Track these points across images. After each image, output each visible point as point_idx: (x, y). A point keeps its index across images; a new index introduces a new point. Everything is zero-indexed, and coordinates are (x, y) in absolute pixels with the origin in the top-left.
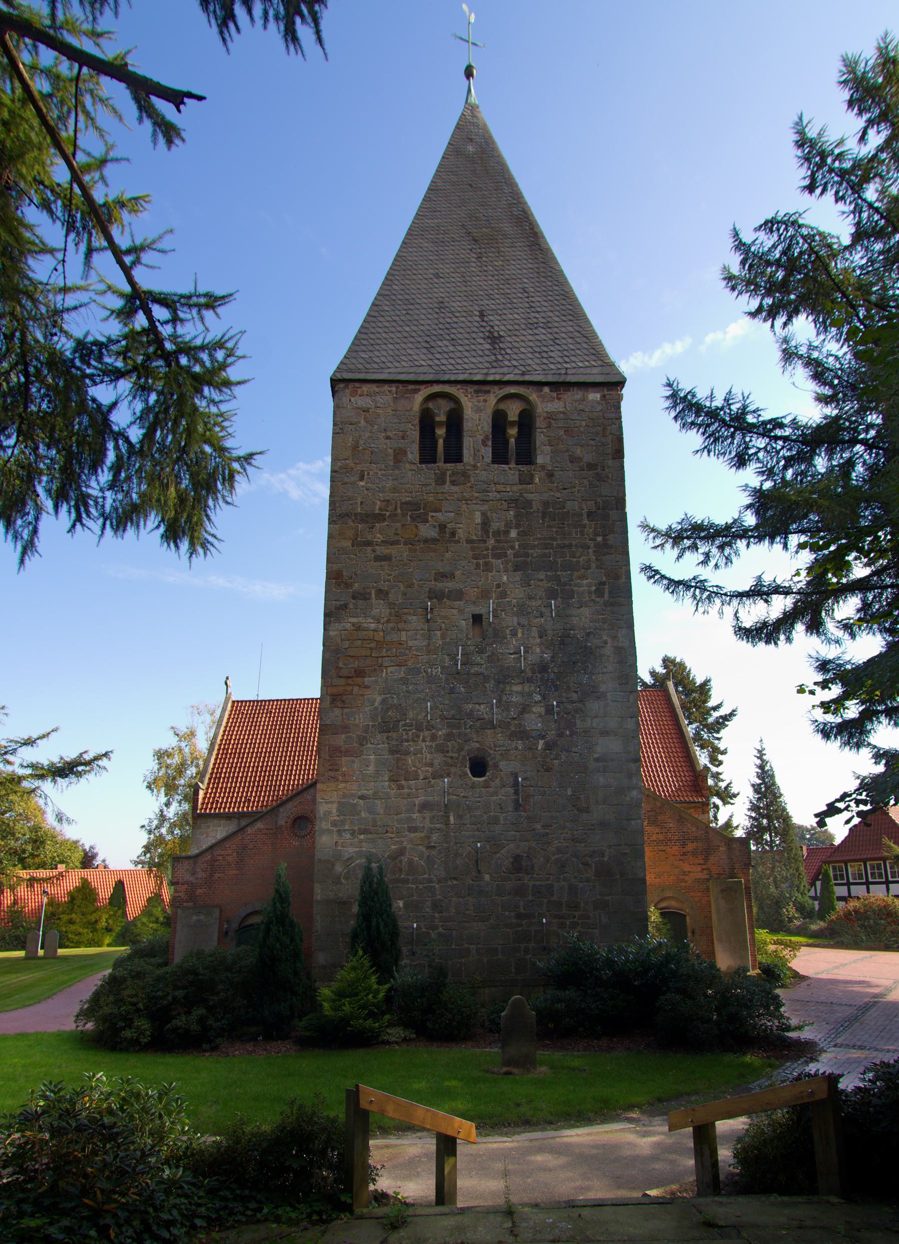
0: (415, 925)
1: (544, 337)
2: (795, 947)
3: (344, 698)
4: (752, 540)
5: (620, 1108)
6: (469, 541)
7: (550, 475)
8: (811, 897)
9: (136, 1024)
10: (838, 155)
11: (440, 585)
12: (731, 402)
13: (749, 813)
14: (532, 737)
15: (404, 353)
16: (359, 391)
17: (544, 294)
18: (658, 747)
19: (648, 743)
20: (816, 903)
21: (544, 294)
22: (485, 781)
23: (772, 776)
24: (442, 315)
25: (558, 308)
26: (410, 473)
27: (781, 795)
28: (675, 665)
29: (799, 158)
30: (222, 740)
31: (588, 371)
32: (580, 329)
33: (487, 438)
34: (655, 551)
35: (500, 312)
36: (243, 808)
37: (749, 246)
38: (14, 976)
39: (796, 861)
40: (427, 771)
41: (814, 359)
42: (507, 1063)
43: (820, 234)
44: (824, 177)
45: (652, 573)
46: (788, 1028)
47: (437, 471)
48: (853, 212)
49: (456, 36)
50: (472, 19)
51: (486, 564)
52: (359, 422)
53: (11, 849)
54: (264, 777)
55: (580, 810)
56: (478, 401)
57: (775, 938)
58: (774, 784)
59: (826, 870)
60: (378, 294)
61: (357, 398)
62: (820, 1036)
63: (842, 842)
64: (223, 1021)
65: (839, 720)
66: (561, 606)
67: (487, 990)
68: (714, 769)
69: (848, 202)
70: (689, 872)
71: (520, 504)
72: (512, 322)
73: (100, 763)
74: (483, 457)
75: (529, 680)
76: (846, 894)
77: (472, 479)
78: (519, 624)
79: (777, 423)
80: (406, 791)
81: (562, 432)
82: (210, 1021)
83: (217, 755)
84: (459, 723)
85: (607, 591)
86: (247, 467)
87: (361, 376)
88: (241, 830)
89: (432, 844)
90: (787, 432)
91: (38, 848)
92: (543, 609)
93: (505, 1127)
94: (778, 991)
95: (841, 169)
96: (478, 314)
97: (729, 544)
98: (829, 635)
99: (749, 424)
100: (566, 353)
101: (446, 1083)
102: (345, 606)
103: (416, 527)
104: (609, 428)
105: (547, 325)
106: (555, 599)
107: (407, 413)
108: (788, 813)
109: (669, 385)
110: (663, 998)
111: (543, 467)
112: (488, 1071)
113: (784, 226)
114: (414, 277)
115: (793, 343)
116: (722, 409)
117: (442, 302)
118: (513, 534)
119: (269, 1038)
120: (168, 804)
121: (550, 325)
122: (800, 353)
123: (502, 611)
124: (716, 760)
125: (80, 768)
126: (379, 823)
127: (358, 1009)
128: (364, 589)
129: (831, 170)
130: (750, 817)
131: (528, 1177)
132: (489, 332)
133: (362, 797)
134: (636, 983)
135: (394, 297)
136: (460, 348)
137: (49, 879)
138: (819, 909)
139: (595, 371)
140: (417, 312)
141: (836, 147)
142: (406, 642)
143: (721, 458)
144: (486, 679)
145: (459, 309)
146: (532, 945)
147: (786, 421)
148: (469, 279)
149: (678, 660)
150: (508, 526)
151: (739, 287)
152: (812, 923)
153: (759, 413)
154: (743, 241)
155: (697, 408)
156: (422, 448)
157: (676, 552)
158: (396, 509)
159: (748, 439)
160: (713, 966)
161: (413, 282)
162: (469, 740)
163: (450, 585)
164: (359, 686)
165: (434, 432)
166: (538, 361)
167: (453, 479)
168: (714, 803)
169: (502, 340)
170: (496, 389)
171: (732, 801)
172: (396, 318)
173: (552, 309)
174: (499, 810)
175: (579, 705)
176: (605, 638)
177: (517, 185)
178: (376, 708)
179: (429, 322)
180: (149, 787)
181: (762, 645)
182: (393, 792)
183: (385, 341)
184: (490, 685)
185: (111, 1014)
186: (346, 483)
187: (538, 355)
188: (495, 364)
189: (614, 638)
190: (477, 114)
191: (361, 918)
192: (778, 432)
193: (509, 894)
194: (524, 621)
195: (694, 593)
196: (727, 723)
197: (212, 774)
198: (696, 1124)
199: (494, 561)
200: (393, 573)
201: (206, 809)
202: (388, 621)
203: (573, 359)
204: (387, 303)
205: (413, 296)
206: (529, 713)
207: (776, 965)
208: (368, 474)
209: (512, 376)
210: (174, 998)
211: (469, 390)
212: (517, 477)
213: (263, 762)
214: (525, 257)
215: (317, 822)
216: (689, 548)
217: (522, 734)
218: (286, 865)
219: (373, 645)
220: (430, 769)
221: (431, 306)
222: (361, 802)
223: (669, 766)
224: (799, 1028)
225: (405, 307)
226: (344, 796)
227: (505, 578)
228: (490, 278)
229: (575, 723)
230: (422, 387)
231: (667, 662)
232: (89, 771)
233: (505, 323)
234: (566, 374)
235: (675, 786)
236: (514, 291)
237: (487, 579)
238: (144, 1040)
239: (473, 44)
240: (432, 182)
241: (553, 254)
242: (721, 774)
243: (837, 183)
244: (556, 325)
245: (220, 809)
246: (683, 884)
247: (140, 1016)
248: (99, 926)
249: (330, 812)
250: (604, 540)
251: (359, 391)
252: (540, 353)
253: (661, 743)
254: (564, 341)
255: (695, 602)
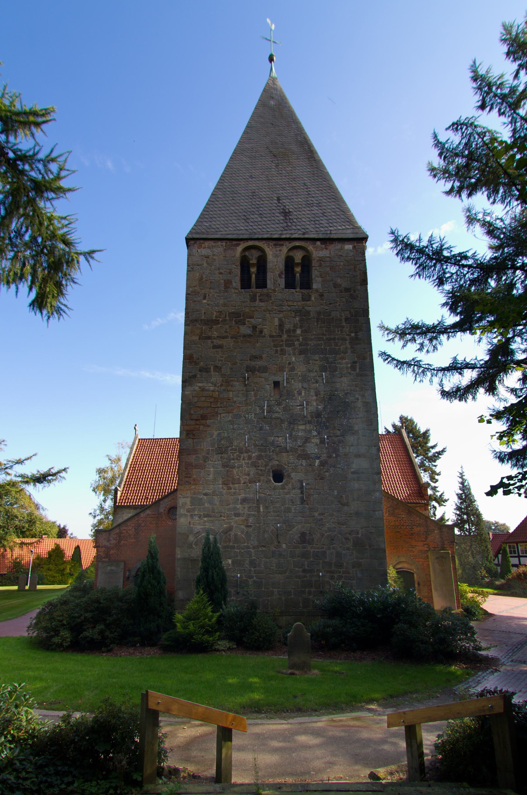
0: (239, 575)
1: (317, 212)
2: (485, 595)
3: (194, 432)
4: (450, 334)
5: (364, 702)
6: (271, 336)
7: (321, 295)
8: (495, 564)
9: (61, 633)
10: (500, 84)
11: (253, 363)
12: (432, 242)
13: (455, 512)
14: (312, 458)
15: (231, 222)
16: (203, 245)
17: (317, 186)
18: (396, 469)
19: (390, 466)
20: (499, 568)
21: (317, 186)
22: (283, 485)
23: (469, 489)
24: (254, 200)
25: (325, 195)
26: (234, 295)
27: (475, 501)
28: (407, 421)
29: (474, 88)
30: (132, 462)
31: (345, 231)
32: (339, 207)
33: (282, 273)
34: (389, 342)
35: (290, 197)
36: (144, 502)
37: (444, 145)
38: (7, 601)
39: (485, 541)
40: (246, 478)
41: (487, 222)
42: (293, 666)
43: (489, 131)
44: (491, 100)
45: (386, 356)
46: (480, 649)
47: (251, 294)
48: (511, 123)
49: (263, 38)
50: (273, 27)
51: (282, 350)
52: (203, 264)
53: (16, 526)
54: (157, 484)
55: (343, 505)
56: (276, 251)
57: (472, 589)
58: (470, 494)
59: (505, 548)
60: (215, 188)
61: (202, 249)
62: (501, 654)
63: (515, 531)
64: (115, 633)
65: (509, 450)
66: (329, 376)
67: (284, 618)
68: (433, 484)
69: (507, 115)
70: (416, 546)
71: (303, 314)
72: (297, 203)
73: (61, 474)
74: (279, 285)
75: (310, 422)
76: (517, 563)
77: (273, 298)
78: (303, 387)
79: (463, 256)
80: (233, 490)
81: (328, 269)
82: (107, 633)
83: (129, 470)
84: (266, 449)
85: (358, 367)
86: (90, 259)
87: (204, 236)
88: (137, 514)
89: (250, 524)
90: (470, 262)
91: (32, 526)
92: (318, 378)
93: (285, 712)
94: (472, 624)
95: (501, 94)
96: (276, 198)
97: (436, 338)
98: (500, 396)
99: (445, 257)
100: (330, 221)
101: (251, 680)
102: (195, 376)
103: (238, 328)
104: (358, 266)
105: (319, 205)
106: (325, 372)
107: (232, 258)
108: (479, 512)
109: (393, 233)
110: (395, 626)
111: (317, 291)
112: (279, 672)
113: (465, 127)
114: (237, 178)
115: (474, 212)
116: (427, 247)
117: (254, 192)
118: (299, 332)
119: (143, 645)
120: (105, 501)
121: (320, 205)
122: (478, 218)
123: (292, 379)
124: (434, 479)
125: (50, 478)
126: (216, 511)
127: (199, 628)
128: (206, 365)
129: (495, 95)
130: (456, 514)
131: (293, 752)
132: (283, 209)
133: (205, 494)
134: (379, 616)
135: (224, 190)
136: (265, 219)
137: (31, 544)
138: (501, 572)
139: (349, 231)
140: (239, 198)
141: (498, 79)
142: (233, 398)
143: (427, 280)
144: (282, 421)
145: (265, 196)
146: (313, 590)
147: (469, 254)
148: (270, 178)
149: (409, 418)
150: (295, 327)
151: (439, 175)
152: (496, 580)
153: (451, 249)
154: (440, 141)
155: (410, 247)
156: (242, 280)
157: (402, 343)
158: (226, 317)
159: (445, 267)
160: (429, 606)
161: (237, 181)
162: (272, 459)
163: (260, 363)
164: (204, 425)
165: (249, 271)
166: (313, 226)
167: (261, 298)
168: (433, 505)
169: (291, 214)
170: (287, 243)
171: (444, 504)
172: (226, 202)
173: (321, 195)
174: (291, 504)
175: (341, 438)
176: (357, 396)
177: (300, 123)
178: (214, 439)
179: (246, 204)
180: (94, 490)
181: (456, 402)
182: (224, 491)
183: (219, 216)
184: (285, 425)
185: (46, 626)
186: (195, 301)
187: (313, 223)
188: (286, 228)
189: (363, 396)
190: (276, 83)
191: (202, 570)
192: (464, 262)
193: (299, 557)
194: (306, 385)
195: (414, 369)
196: (440, 456)
197: (126, 482)
198: (406, 724)
199: (286, 348)
200: (224, 356)
201: (122, 503)
202: (221, 385)
203: (335, 224)
204: (221, 193)
205: (236, 189)
206: (309, 442)
207: (472, 607)
208: (209, 296)
209: (297, 235)
210: (85, 618)
211: (270, 244)
212: (300, 296)
213: (156, 475)
214: (305, 165)
215: (178, 509)
216: (410, 340)
217: (305, 456)
218: (155, 535)
219: (212, 400)
220: (248, 477)
221: (247, 194)
222: (205, 497)
223: (403, 481)
224: (488, 649)
225: (231, 195)
226: (195, 494)
227: (294, 359)
228: (284, 177)
229: (339, 449)
230: (241, 242)
231: (403, 419)
232: (55, 480)
233: (293, 204)
234: (331, 233)
235: (407, 493)
236: (299, 185)
237: (282, 359)
238: (65, 644)
239: (274, 42)
240: (249, 122)
241: (322, 163)
242: (437, 487)
243: (499, 103)
244: (325, 204)
245: (130, 503)
246: (412, 553)
247: (64, 629)
248: (65, 572)
249: (186, 503)
250: (356, 335)
251: (203, 245)
252: (314, 221)
253: (398, 467)
254: (330, 214)
255: (414, 375)
